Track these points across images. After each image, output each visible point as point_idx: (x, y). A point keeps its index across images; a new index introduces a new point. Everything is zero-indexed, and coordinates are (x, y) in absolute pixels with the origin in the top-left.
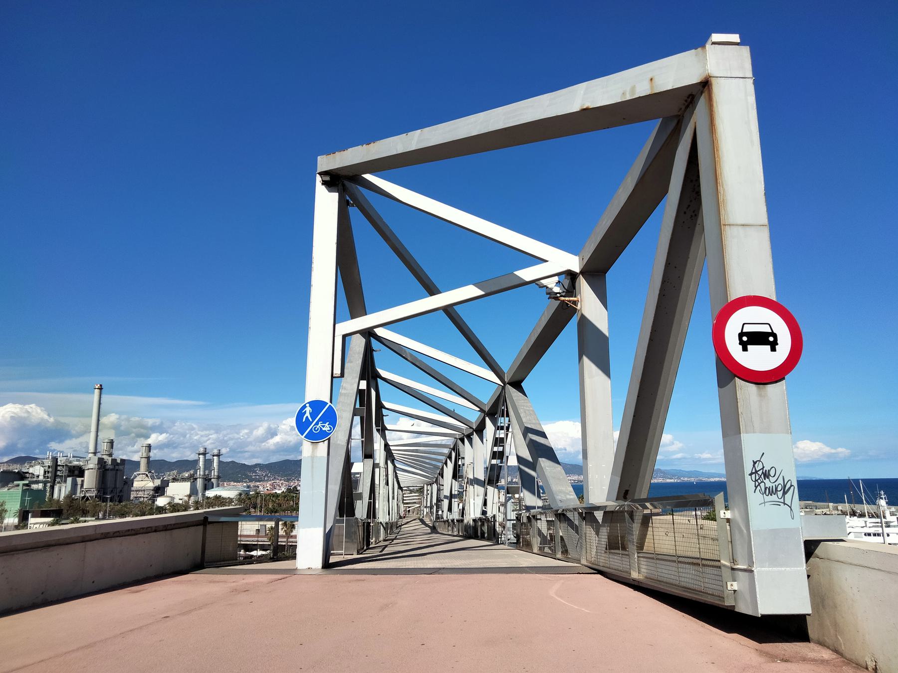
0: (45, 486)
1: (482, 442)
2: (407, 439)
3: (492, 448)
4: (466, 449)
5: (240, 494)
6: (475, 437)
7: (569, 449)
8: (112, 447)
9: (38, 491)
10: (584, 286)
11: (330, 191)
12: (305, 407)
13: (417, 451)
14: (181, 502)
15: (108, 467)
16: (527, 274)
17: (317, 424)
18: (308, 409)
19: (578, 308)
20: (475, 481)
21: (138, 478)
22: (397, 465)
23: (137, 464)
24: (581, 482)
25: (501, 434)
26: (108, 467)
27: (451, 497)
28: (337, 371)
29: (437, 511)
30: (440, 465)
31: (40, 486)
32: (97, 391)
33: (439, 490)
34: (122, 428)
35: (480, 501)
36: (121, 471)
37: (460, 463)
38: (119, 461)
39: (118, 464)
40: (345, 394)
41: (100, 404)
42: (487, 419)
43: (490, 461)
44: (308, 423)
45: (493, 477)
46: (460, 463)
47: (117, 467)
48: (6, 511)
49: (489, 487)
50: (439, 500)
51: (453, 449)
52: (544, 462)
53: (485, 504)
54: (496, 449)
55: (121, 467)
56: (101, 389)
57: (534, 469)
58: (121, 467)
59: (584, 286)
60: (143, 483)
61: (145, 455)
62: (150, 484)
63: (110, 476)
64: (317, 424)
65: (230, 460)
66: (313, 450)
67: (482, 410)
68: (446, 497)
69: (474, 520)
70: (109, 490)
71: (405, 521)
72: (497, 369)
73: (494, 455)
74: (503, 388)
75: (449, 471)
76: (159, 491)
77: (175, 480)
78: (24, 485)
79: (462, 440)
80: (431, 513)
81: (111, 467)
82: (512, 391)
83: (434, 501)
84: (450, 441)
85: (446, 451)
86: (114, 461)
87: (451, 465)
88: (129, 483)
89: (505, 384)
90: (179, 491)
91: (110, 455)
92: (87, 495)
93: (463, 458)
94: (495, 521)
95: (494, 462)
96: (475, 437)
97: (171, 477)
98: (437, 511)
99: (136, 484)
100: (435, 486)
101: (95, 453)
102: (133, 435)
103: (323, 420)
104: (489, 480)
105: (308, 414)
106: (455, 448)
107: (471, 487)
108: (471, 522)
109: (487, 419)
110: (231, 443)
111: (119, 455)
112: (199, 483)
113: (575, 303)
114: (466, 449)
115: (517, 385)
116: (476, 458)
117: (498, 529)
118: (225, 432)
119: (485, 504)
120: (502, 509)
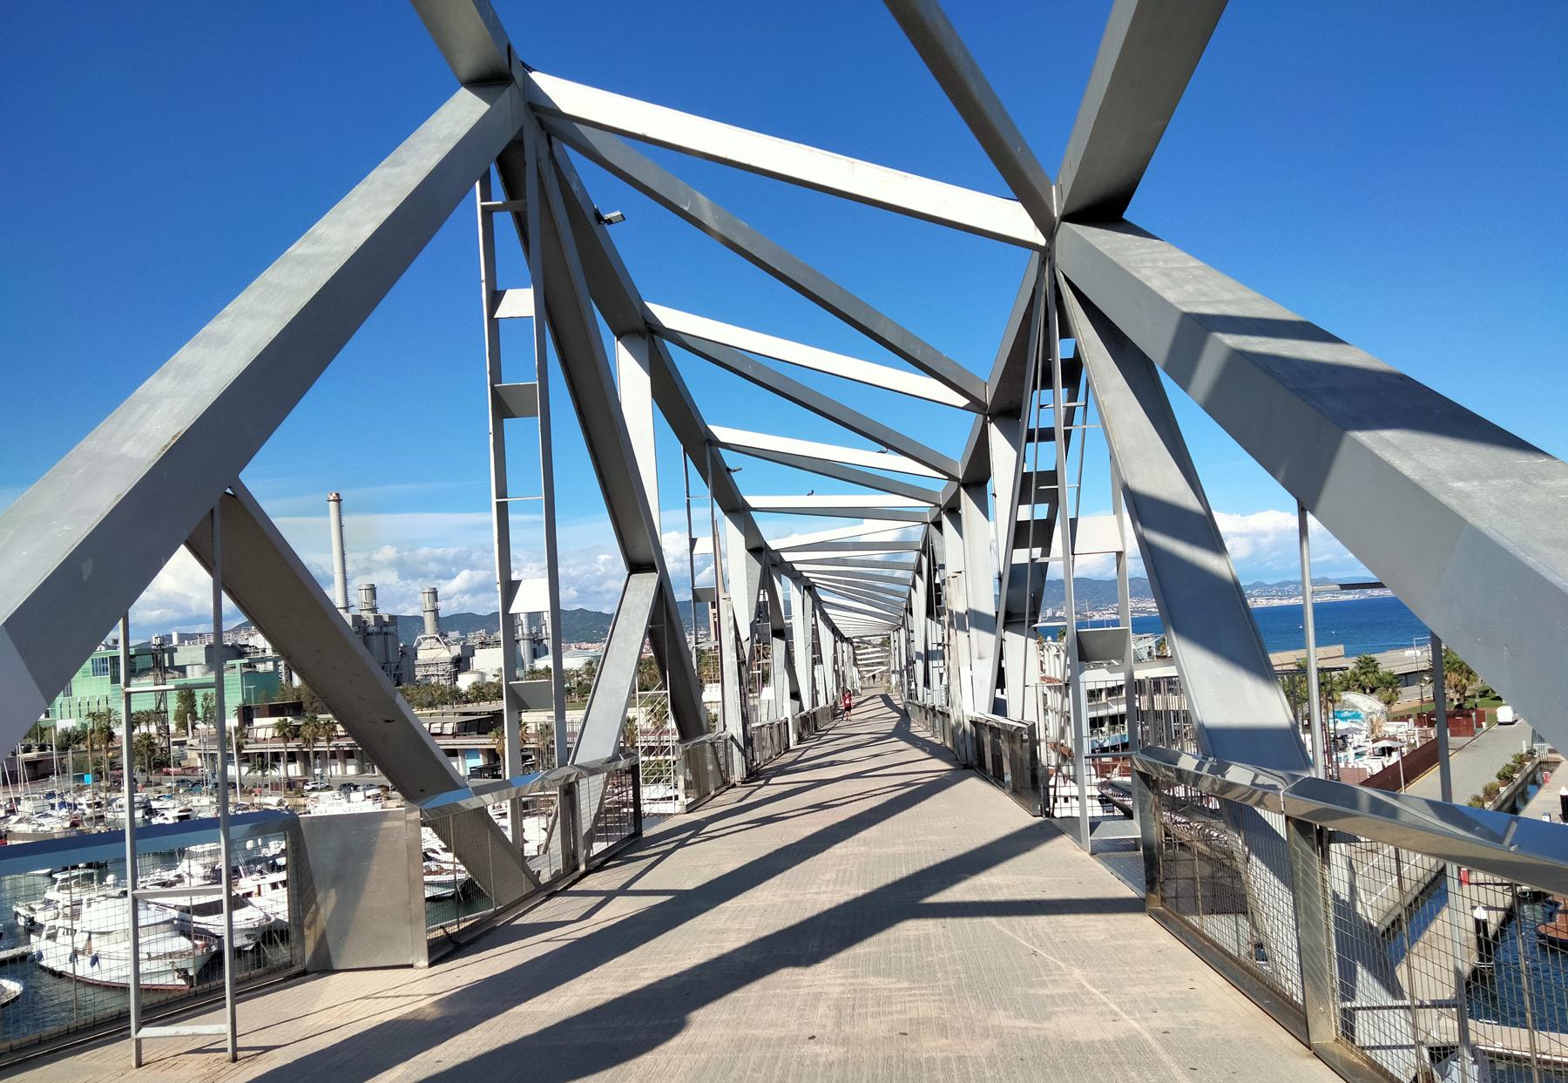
0: (276, 666)
1: (985, 512)
3: (1013, 511)
4: (949, 544)
5: (590, 663)
6: (967, 505)
8: (436, 600)
9: (266, 673)
13: (844, 562)
14: (495, 680)
20: (977, 620)
21: (424, 645)
22: (823, 598)
23: (420, 620)
25: (1043, 457)
26: (370, 630)
27: (928, 656)
29: (909, 683)
31: (270, 666)
32: (333, 505)
33: (908, 641)
35: (987, 673)
37: (938, 581)
38: (386, 619)
39: (386, 624)
41: (341, 526)
42: (994, 430)
43: (1009, 556)
45: (1023, 601)
46: (938, 581)
49: (1008, 635)
50: (910, 662)
51: (923, 552)
53: (1000, 682)
54: (1024, 513)
55: (391, 629)
56: (338, 501)
58: (391, 629)
60: (432, 654)
61: (429, 607)
62: (446, 654)
65: (578, 607)
67: (975, 405)
68: (919, 655)
69: (974, 723)
73: (1021, 534)
75: (919, 600)
76: (461, 664)
77: (484, 645)
78: (245, 665)
79: (938, 525)
80: (902, 684)
83: (904, 663)
84: (916, 532)
85: (912, 557)
86: (378, 619)
87: (921, 585)
88: (410, 654)
89: (1049, 230)
90: (489, 662)
91: (374, 610)
93: (942, 566)
94: (1035, 743)
95: (1021, 556)
96: (967, 505)
97: (477, 641)
98: (909, 683)
99: (423, 656)
101: (346, 608)
104: (1008, 615)
106: (927, 540)
107: (962, 635)
108: (968, 725)
109: (994, 430)
111: (385, 612)
112: (524, 648)
114: (949, 544)
116: (977, 556)
117: (1047, 756)
119: (1000, 682)
120: (1055, 699)
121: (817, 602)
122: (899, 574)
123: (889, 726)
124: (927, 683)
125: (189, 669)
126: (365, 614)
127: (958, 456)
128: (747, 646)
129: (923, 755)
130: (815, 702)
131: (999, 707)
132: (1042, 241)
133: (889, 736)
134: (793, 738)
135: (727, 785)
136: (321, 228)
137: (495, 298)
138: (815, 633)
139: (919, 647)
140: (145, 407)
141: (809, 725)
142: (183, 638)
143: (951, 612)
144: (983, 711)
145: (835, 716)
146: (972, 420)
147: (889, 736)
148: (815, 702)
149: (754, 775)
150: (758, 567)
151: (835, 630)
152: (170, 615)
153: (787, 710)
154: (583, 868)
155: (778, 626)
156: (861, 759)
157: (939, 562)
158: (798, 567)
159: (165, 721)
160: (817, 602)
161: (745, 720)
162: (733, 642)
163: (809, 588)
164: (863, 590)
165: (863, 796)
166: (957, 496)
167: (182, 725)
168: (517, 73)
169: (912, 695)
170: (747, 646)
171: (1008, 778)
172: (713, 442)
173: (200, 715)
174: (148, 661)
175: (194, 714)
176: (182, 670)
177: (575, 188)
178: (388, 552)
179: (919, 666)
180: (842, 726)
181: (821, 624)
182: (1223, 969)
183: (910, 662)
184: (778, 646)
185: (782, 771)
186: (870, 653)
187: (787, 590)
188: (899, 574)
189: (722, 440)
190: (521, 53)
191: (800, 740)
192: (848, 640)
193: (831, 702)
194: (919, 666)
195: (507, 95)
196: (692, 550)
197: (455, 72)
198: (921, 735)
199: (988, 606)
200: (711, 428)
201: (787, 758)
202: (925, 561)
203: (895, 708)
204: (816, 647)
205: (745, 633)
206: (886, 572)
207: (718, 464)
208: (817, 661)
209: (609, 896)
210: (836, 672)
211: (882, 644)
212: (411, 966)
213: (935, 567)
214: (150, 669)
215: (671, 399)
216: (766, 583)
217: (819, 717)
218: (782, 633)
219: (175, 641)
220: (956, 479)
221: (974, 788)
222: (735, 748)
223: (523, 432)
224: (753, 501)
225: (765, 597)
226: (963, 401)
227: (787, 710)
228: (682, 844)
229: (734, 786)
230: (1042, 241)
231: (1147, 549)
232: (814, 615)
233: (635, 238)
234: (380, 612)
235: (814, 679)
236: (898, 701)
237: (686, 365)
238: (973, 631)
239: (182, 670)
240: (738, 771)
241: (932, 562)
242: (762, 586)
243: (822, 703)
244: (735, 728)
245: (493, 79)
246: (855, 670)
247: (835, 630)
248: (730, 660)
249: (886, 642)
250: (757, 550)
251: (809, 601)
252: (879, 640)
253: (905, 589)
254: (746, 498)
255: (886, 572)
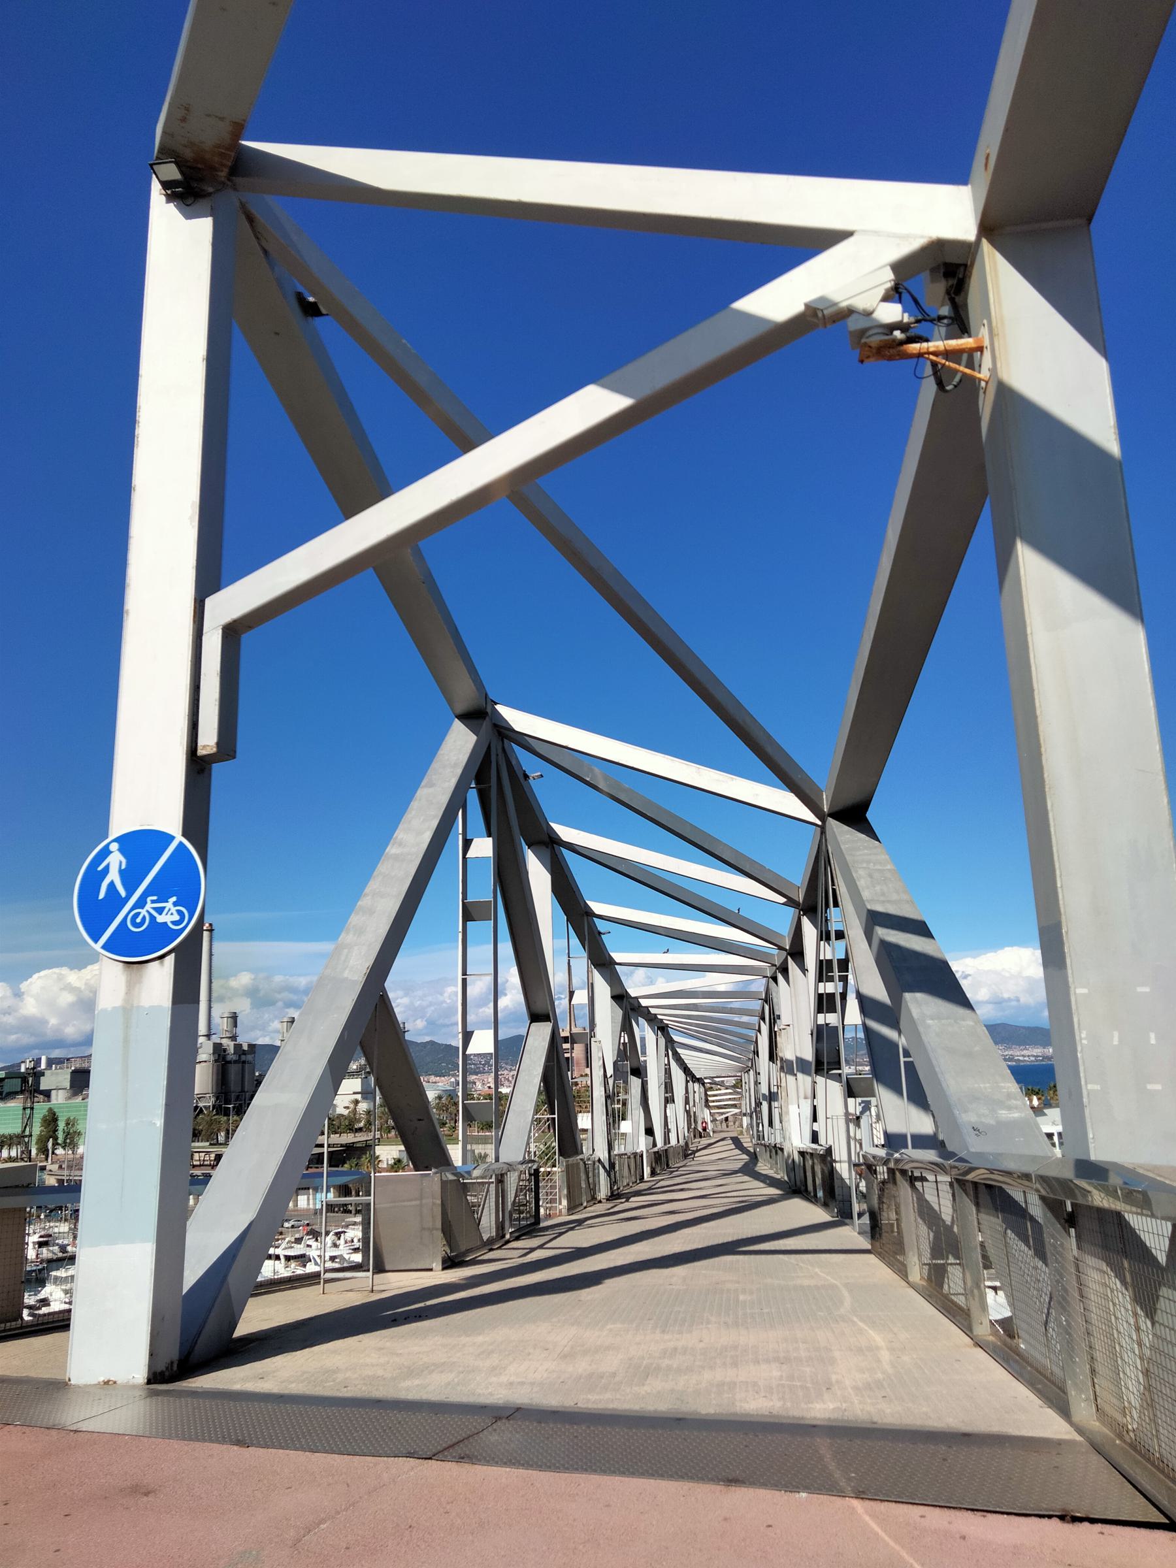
2: (665, 983)
3: (817, 988)
6: (792, 966)
7: (1025, 999)
8: (236, 1026)
10: (1005, 288)
11: (188, 216)
12: (106, 852)
13: (695, 1007)
14: (346, 1112)
15: (229, 1058)
16: (777, 301)
17: (141, 903)
18: (116, 860)
19: (984, 374)
20: (803, 1066)
22: (676, 1038)
24: (1049, 1058)
26: (229, 1058)
28: (208, 740)
30: (752, 1034)
33: (757, 1083)
34: (262, 993)
36: (249, 1063)
38: (245, 1048)
40: (396, 858)
43: (816, 1019)
44: (115, 902)
47: (243, 1058)
48: (79, 1134)
50: (758, 1104)
52: (920, 1006)
55: (249, 1057)
57: (895, 1024)
58: (249, 1057)
59: (1005, 288)
63: (233, 1070)
64: (141, 903)
65: (427, 1039)
66: (131, 986)
69: (802, 1154)
70: (233, 1096)
71: (704, 1141)
72: (797, 778)
74: (823, 829)
79: (775, 979)
81: (235, 1058)
82: (843, 835)
84: (758, 985)
85: (756, 1005)
86: (238, 1047)
87: (765, 1028)
91: (234, 1038)
92: (201, 1105)
96: (792, 966)
100: (751, 1072)
101: (208, 1036)
102: (280, 1004)
103: (160, 890)
105: (114, 876)
107: (790, 1078)
108: (796, 1157)
110: (430, 1011)
111: (244, 1040)
113: (971, 356)
115: (855, 815)
118: (420, 993)
121: (670, 1042)
122: (745, 1019)
123: (739, 1165)
124: (771, 1124)
125: (53, 1093)
126: (225, 1042)
127: (784, 930)
128: (611, 1081)
129: (762, 1185)
130: (667, 1140)
131: (815, 1138)
132: (819, 823)
133: (735, 1172)
134: (647, 1171)
135: (594, 1199)
136: (400, 834)
137: (467, 843)
138: (668, 1072)
139: (764, 1090)
140: (346, 951)
141: (661, 1160)
142: (50, 1062)
143: (782, 1059)
144: (805, 1144)
145: (686, 1156)
146: (791, 912)
147: (735, 1172)
148: (667, 1140)
149: (614, 1196)
150: (620, 1012)
151: (686, 1070)
152: (27, 1040)
153: (642, 1145)
154: (508, 1236)
155: (635, 1065)
156: (707, 1187)
157: (777, 1013)
158: (653, 1011)
159: (27, 1145)
160: (670, 1042)
161: (610, 1147)
162: (602, 1078)
163: (662, 1029)
164: (716, 1031)
165: (705, 1207)
166: (786, 959)
167: (44, 1150)
168: (489, 710)
169: (760, 1137)
170: (611, 1081)
171: (820, 1194)
172: (590, 914)
173: (60, 1141)
174: (16, 1084)
175: (56, 1139)
176: (47, 1094)
177: (514, 763)
178: (244, 979)
179: (765, 1105)
180: (692, 1165)
181: (673, 1064)
182: (949, 1312)
183: (758, 1104)
184: (635, 1083)
185: (638, 1193)
186: (721, 1095)
187: (644, 1032)
188: (745, 1019)
189: (597, 912)
190: (491, 696)
191: (653, 1173)
192: (700, 1081)
193: (682, 1142)
194: (765, 1105)
195: (486, 725)
196: (570, 1001)
197: (450, 702)
198: (764, 1172)
199: (809, 1055)
200: (590, 903)
201: (643, 1186)
202: (767, 1007)
203: (744, 1150)
204: (668, 1087)
205: (610, 1072)
206: (736, 1018)
207: (592, 927)
208: (669, 1100)
209: (532, 1250)
210: (688, 1112)
211: (735, 1086)
212: (431, 1270)
213: (774, 1019)
214: (16, 1093)
215: (566, 892)
216: (627, 1027)
217: (671, 1155)
218: (639, 1071)
219: (43, 1066)
220: (785, 950)
221: (797, 1203)
222: (602, 1170)
223: (481, 929)
224: (617, 957)
225: (625, 1038)
226: (783, 900)
227: (642, 1145)
228: (572, 1229)
229: (600, 1202)
230: (819, 823)
231: (866, 1028)
232: (667, 1055)
233: (547, 789)
234: (239, 1040)
235: (666, 1117)
236: (748, 1143)
237: (581, 872)
238: (800, 1075)
239: (47, 1094)
240: (603, 1191)
241: (772, 1011)
242: (623, 1029)
243: (673, 1142)
244: (602, 1153)
245: (478, 715)
246: (707, 1111)
247: (686, 1070)
248: (599, 1094)
249: (738, 1084)
250: (620, 997)
251: (662, 1041)
252: (732, 1081)
253: (752, 1034)
254: (612, 954)
255: (736, 1018)
